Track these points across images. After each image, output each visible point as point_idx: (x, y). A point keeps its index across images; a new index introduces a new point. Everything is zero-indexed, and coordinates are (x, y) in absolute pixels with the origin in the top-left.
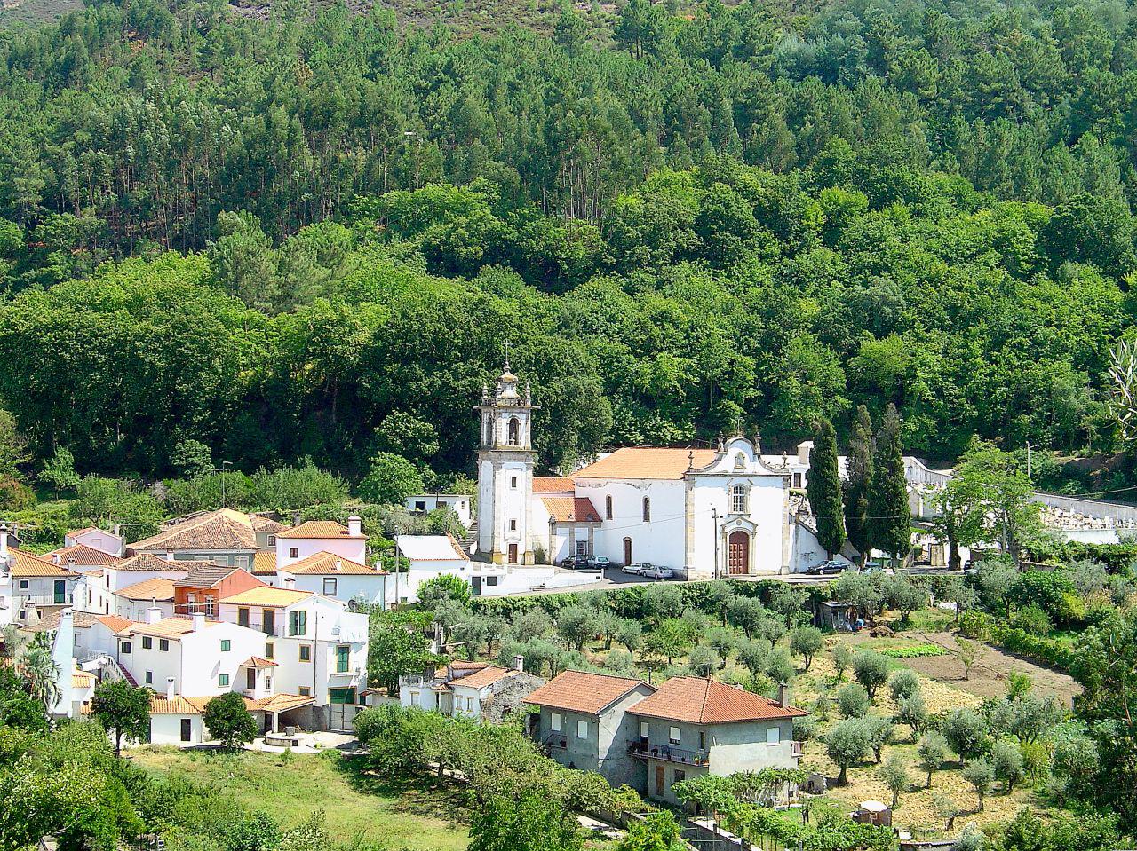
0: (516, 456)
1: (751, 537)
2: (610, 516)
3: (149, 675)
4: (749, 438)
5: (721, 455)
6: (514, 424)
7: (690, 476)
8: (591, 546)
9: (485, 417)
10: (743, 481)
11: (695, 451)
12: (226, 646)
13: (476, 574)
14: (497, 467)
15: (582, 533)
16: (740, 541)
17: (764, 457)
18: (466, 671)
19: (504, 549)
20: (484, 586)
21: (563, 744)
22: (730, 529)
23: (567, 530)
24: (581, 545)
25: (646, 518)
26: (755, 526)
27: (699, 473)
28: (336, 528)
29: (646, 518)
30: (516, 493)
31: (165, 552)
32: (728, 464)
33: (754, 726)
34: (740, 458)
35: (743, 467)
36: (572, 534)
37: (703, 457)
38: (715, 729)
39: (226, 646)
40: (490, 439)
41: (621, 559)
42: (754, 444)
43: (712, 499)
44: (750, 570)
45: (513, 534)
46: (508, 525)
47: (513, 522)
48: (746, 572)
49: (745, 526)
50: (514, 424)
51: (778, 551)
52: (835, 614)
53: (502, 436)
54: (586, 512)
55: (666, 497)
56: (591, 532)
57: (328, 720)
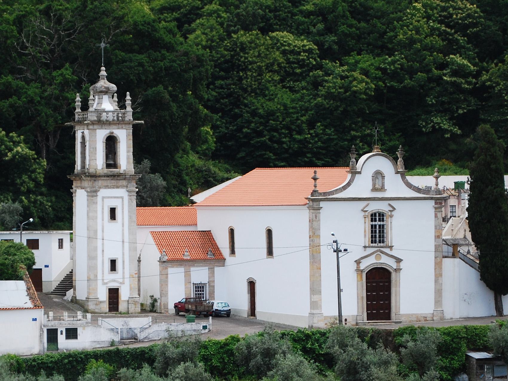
0: (114, 182)
1: (393, 275)
2: (233, 252)
3: (61, 246)
4: (390, 152)
5: (355, 173)
6: (111, 143)
7: (316, 200)
9: (79, 135)
10: (382, 207)
11: (318, 170)
14: (93, 193)
17: (409, 178)
20: (61, 339)
22: (366, 264)
23: (182, 270)
24: (199, 288)
25: (270, 252)
26: (399, 260)
29: (270, 252)
30: (117, 225)
32: (362, 186)
34: (378, 175)
35: (382, 189)
36: (187, 275)
37: (330, 177)
41: (244, 306)
42: (396, 159)
43: (346, 226)
44: (393, 315)
45: (113, 276)
46: (108, 265)
48: (387, 316)
50: (111, 143)
52: (482, 368)
53: (98, 161)
54: (209, 250)
55: (291, 227)
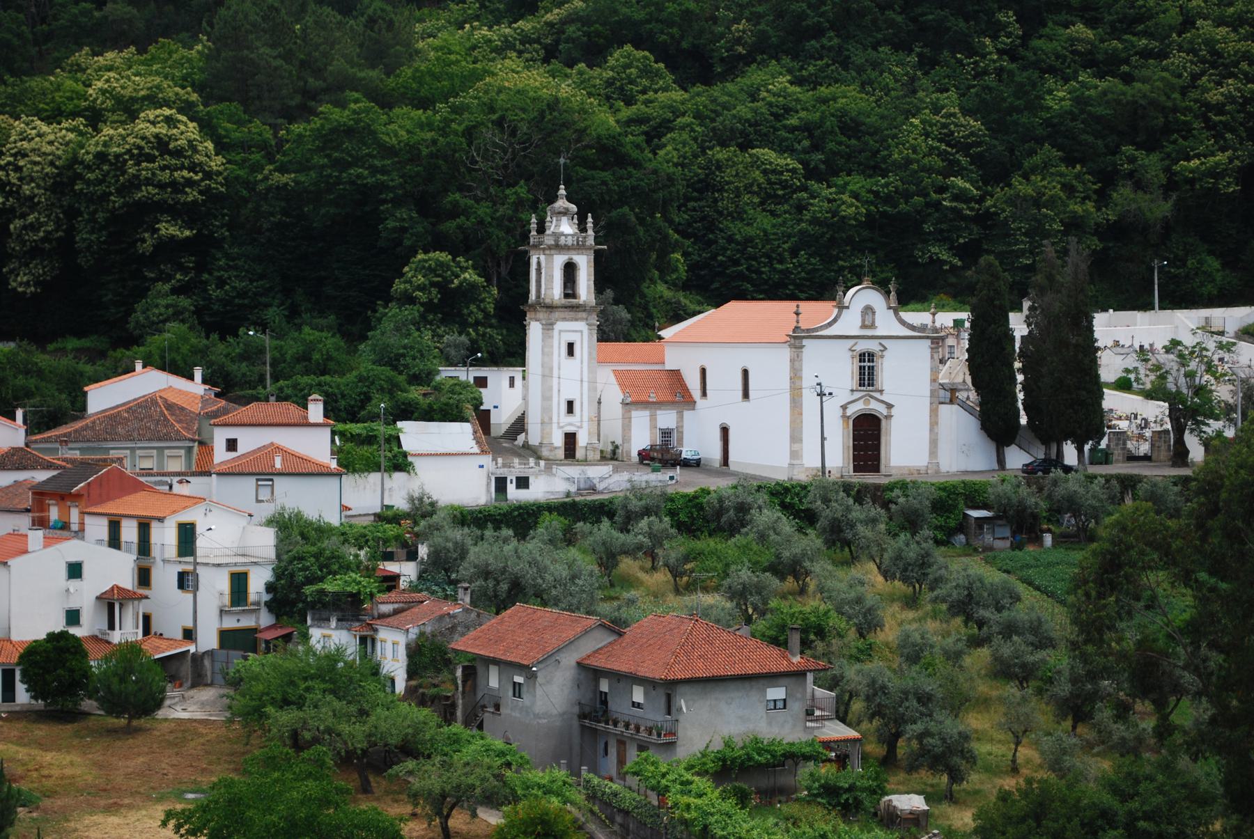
0: (572, 314)
1: (884, 423)
2: (704, 394)
6: (570, 270)
7: (798, 338)
8: (681, 433)
10: (872, 346)
12: (75, 570)
13: (502, 472)
14: (548, 327)
15: (667, 419)
16: (867, 434)
18: (396, 606)
19: (559, 441)
20: (511, 489)
21: (497, 707)
24: (666, 433)
25: (746, 395)
26: (890, 406)
27: (811, 334)
28: (292, 410)
29: (746, 395)
31: (57, 445)
32: (850, 323)
33: (747, 684)
34: (868, 310)
36: (653, 419)
37: (814, 312)
38: (682, 689)
39: (75, 570)
40: (538, 296)
42: (888, 293)
43: (832, 367)
44: (882, 467)
45: (570, 419)
46: (564, 407)
47: (570, 405)
49: (876, 407)
50: (570, 270)
51: (931, 440)
52: (981, 528)
53: (555, 290)
54: (676, 393)
55: (771, 367)
56: (681, 417)
57: (209, 674)
